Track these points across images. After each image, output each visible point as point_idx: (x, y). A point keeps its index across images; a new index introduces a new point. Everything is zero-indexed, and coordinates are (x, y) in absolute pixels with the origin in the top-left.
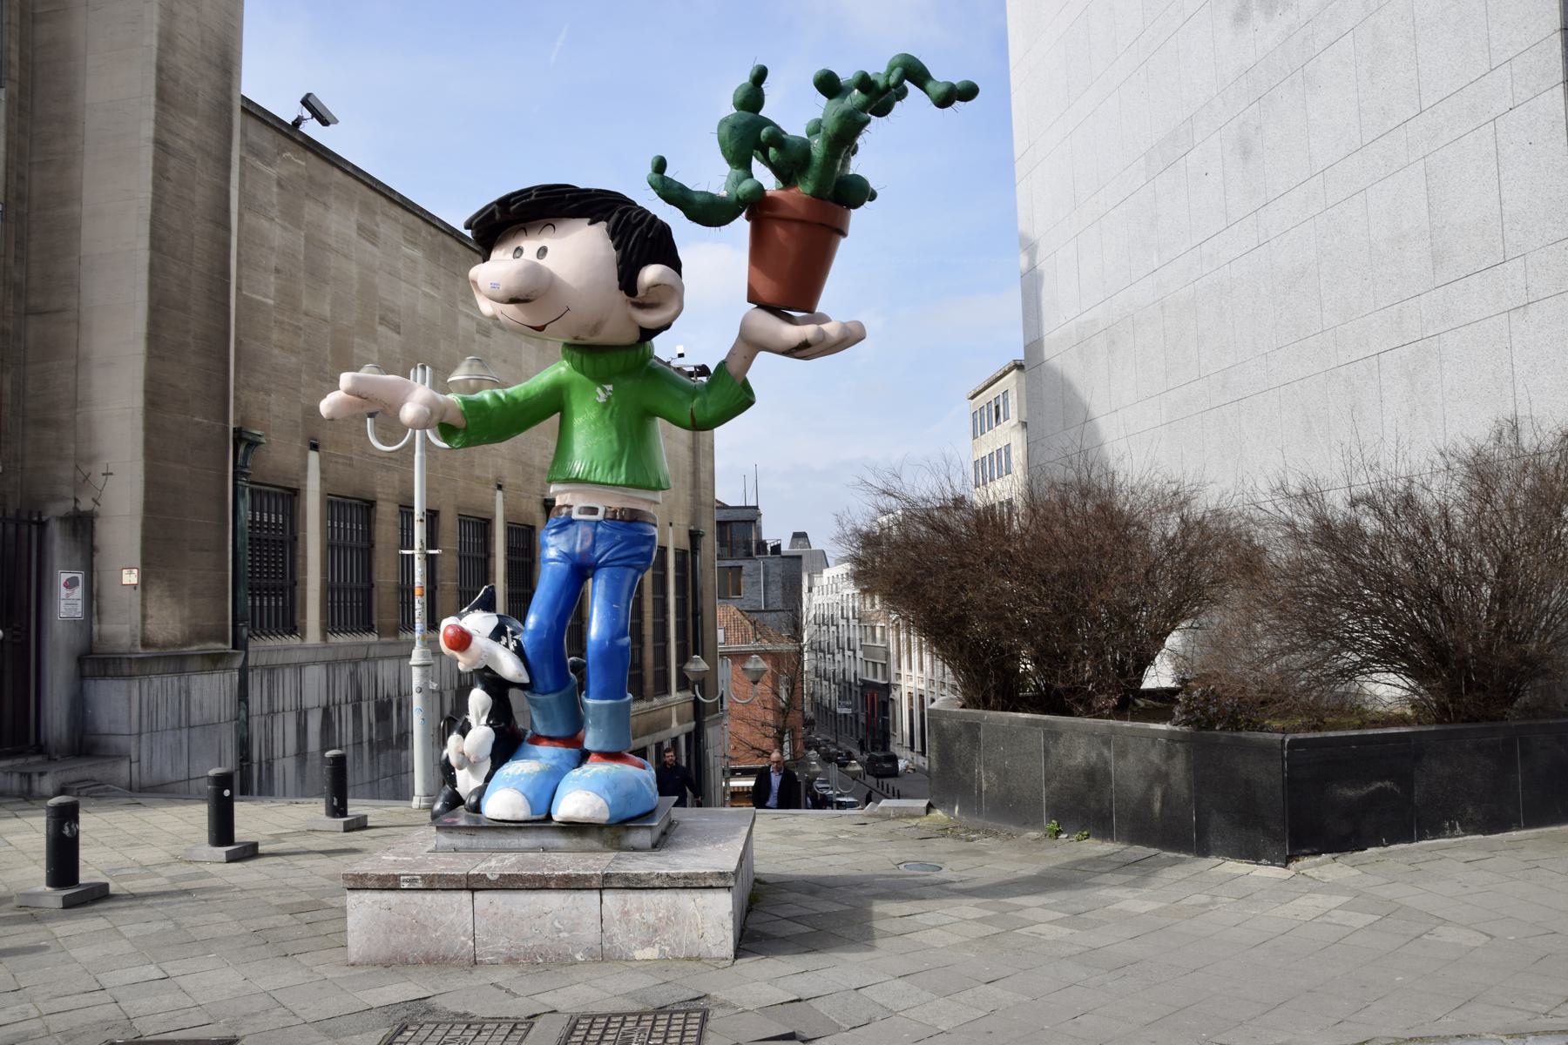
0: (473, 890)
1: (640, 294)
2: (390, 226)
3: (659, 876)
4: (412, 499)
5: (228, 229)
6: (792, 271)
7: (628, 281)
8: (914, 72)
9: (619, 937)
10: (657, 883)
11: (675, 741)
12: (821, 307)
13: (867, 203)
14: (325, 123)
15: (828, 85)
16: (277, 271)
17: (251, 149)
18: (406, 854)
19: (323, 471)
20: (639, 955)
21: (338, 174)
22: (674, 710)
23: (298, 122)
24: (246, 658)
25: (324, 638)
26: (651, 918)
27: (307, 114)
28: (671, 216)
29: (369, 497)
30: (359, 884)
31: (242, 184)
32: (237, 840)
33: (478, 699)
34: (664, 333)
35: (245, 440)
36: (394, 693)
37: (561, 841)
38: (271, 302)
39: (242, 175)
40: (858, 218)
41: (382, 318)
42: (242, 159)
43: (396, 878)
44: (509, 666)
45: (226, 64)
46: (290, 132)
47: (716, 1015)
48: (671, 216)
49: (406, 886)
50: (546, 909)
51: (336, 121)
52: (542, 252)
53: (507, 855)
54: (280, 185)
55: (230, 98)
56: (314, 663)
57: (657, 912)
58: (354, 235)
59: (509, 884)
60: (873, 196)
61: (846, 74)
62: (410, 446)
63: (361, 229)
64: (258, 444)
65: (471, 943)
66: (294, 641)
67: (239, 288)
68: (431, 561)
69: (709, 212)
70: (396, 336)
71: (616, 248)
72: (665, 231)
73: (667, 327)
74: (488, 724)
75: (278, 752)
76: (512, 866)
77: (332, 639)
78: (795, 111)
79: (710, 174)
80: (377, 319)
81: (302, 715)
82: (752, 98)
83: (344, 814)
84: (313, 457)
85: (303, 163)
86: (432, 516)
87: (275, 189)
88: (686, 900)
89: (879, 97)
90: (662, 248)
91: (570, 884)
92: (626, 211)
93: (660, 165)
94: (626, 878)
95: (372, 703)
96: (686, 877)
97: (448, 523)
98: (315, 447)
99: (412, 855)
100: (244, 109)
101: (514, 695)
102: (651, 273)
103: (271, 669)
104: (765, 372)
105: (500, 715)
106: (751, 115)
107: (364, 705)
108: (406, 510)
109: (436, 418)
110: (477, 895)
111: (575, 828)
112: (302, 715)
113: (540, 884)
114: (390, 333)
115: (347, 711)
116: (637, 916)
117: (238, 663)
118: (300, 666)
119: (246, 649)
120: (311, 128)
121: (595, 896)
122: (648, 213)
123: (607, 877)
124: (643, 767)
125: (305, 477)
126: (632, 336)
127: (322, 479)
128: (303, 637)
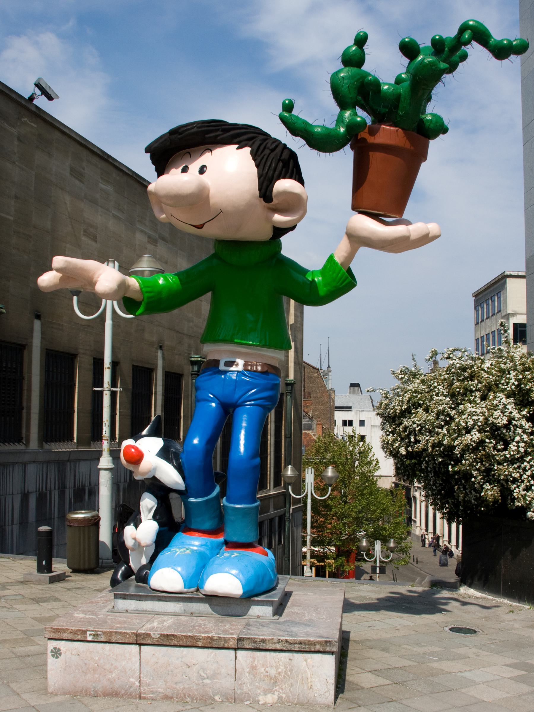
0: (140, 645)
1: (275, 201)
2: (91, 169)
3: (279, 641)
6: (385, 186)
7: (265, 191)
8: (481, 36)
10: (279, 647)
11: (271, 521)
13: (441, 136)
14: (50, 98)
15: (409, 50)
16: (16, 197)
18: (92, 613)
19: (43, 333)
20: (262, 699)
21: (58, 135)
23: (31, 99)
25: (41, 445)
27: (38, 92)
28: (296, 144)
33: (148, 503)
36: (87, 484)
37: (205, 607)
38: (11, 218)
43: (84, 632)
44: (170, 475)
48: (296, 144)
49: (90, 638)
50: (194, 661)
51: (58, 97)
52: (202, 170)
54: (19, 139)
56: (34, 462)
57: (277, 668)
59: (167, 641)
60: (445, 130)
61: (424, 42)
62: (102, 318)
63: (72, 170)
65: (137, 684)
66: (20, 447)
68: (113, 395)
69: (323, 143)
70: (93, 243)
71: (257, 166)
72: (293, 156)
73: (293, 228)
75: (7, 524)
76: (169, 627)
77: (46, 446)
78: (386, 66)
80: (82, 233)
81: (25, 496)
82: (354, 59)
83: (50, 570)
84: (37, 324)
85: (33, 126)
86: (115, 364)
87: (16, 143)
88: (300, 660)
89: (449, 54)
90: (291, 168)
91: (211, 645)
92: (265, 140)
93: (288, 107)
95: (72, 491)
97: (126, 368)
98: (38, 317)
99: (96, 614)
101: (173, 496)
102: (284, 185)
104: (365, 263)
105: (163, 515)
106: (355, 70)
107: (67, 491)
110: (142, 647)
111: (212, 599)
112: (25, 496)
114: (90, 242)
115: (56, 494)
116: (262, 670)
118: (24, 465)
120: (41, 102)
121: (232, 652)
122: (280, 142)
123: (240, 640)
125: (32, 337)
127: (42, 338)
128: (27, 444)
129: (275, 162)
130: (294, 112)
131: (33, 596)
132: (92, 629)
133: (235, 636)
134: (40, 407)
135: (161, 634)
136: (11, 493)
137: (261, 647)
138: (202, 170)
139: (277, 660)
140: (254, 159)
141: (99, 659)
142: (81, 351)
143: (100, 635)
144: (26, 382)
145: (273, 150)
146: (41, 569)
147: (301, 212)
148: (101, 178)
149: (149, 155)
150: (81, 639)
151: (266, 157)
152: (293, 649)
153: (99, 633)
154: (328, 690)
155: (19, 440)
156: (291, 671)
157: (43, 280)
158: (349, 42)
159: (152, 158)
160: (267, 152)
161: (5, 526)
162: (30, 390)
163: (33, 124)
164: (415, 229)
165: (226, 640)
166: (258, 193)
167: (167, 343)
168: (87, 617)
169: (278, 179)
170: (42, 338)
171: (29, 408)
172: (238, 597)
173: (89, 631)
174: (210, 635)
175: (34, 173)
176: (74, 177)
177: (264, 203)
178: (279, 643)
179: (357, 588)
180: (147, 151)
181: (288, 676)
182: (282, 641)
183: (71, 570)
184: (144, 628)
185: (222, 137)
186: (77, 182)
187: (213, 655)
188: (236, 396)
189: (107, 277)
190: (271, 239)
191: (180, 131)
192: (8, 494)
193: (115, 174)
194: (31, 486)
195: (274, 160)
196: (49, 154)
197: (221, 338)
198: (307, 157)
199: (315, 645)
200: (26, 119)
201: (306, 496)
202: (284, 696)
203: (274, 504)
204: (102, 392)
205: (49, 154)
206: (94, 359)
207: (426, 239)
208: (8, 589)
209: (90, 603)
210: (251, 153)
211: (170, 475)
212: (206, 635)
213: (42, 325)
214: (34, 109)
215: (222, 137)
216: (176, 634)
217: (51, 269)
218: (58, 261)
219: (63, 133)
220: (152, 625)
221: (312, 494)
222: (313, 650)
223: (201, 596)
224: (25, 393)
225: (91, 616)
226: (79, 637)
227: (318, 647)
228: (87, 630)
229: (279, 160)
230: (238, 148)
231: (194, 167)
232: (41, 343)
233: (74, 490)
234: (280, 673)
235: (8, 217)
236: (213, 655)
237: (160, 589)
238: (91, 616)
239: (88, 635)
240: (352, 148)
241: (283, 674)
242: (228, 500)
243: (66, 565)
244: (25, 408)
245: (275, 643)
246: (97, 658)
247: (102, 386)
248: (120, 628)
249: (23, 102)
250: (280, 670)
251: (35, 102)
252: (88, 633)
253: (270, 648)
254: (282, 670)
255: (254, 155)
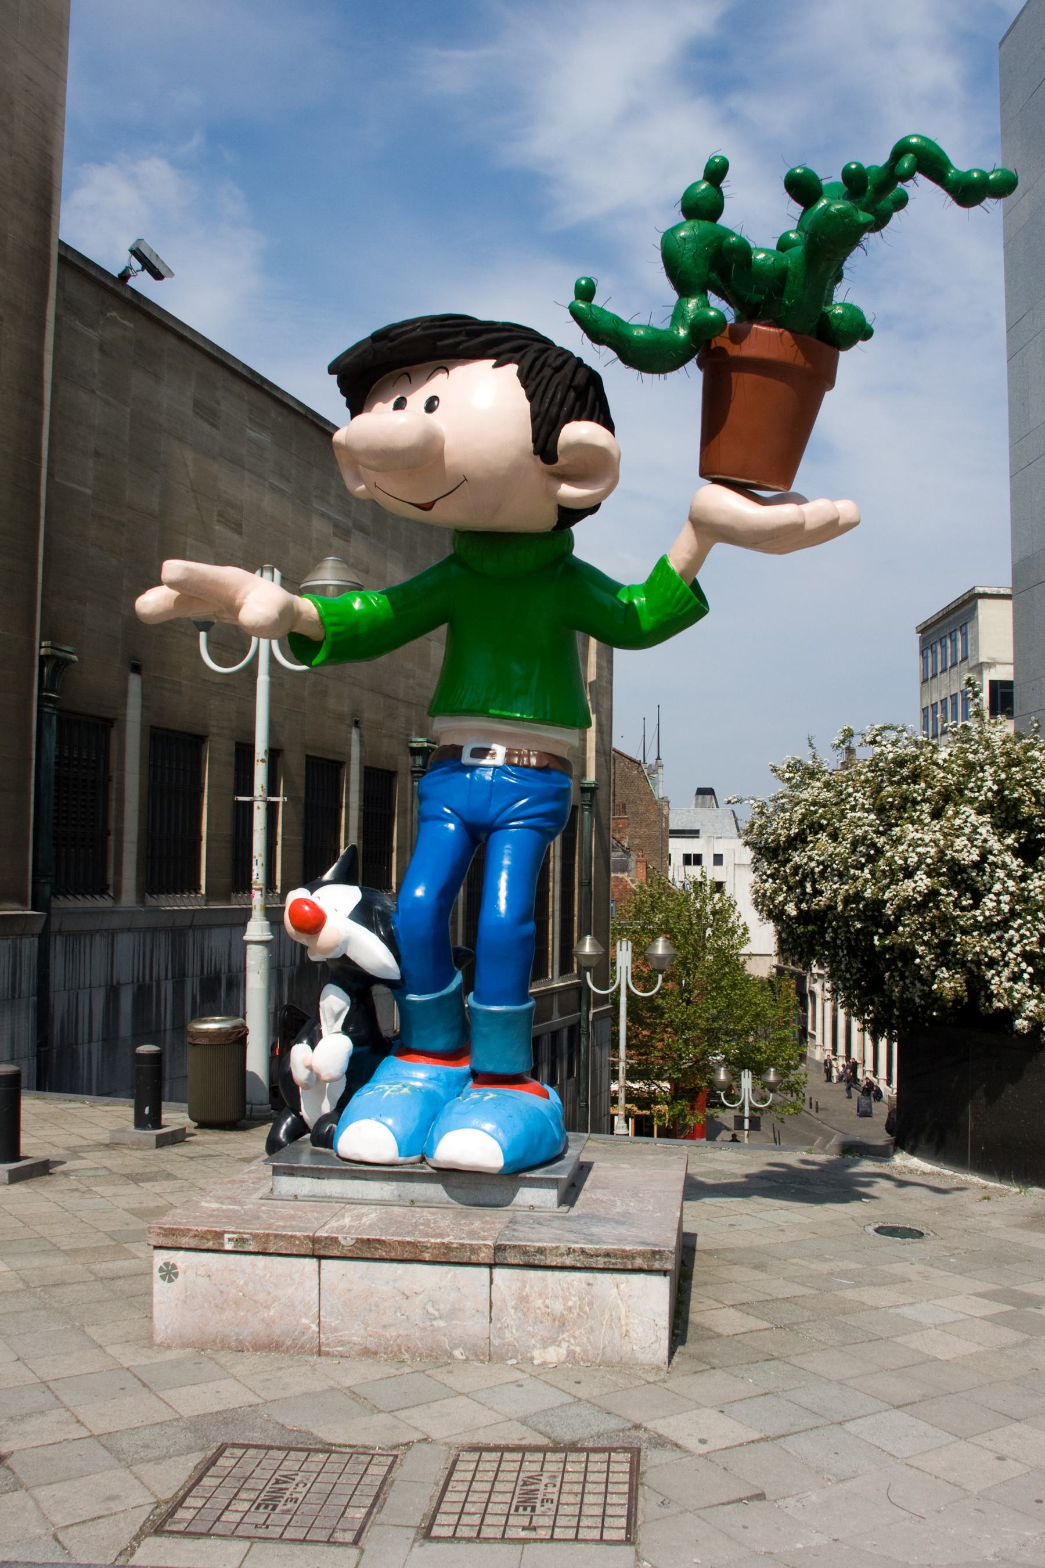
0: (320, 1258)
1: (562, 460)
3: (569, 1251)
4: (252, 734)
5: (41, 403)
7: (544, 444)
8: (931, 163)
9: (512, 1328)
10: (568, 1261)
12: (797, 486)
13: (860, 343)
14: (158, 276)
15: (802, 188)
16: (97, 454)
17: (64, 302)
18: (233, 1200)
19: (145, 697)
20: (538, 1356)
21: (172, 342)
22: (556, 999)
23: (124, 276)
24: (48, 922)
25: (141, 899)
26: (558, 1307)
27: (137, 265)
28: (599, 359)
29: (198, 730)
30: (172, 1240)
31: (56, 349)
32: (24, 1151)
33: (334, 1003)
34: (589, 518)
35: (56, 666)
36: (224, 968)
38: (88, 491)
39: (57, 336)
40: (850, 363)
41: (220, 515)
42: (58, 318)
43: (219, 1235)
44: (373, 953)
45: (43, 199)
46: (113, 290)
47: (652, 1458)
48: (599, 359)
49: (229, 1246)
51: (172, 274)
53: (365, 1209)
54: (102, 350)
55: (47, 244)
56: (129, 930)
57: (566, 1299)
58: (190, 413)
59: (368, 1251)
61: (830, 175)
62: (252, 670)
63: (198, 405)
64: (68, 662)
65: (314, 1327)
66: (103, 903)
67: (50, 474)
68: (271, 809)
69: (649, 356)
70: (236, 537)
71: (530, 397)
72: (594, 380)
73: (594, 509)
74: (345, 1029)
77: (151, 901)
78: (761, 219)
79: (647, 301)
80: (215, 517)
81: (113, 991)
82: (703, 207)
83: (157, 1124)
84: (135, 682)
86: (274, 754)
87: (97, 355)
89: (874, 195)
90: (591, 400)
93: (586, 292)
94: (523, 1250)
95: (197, 981)
96: (607, 1255)
97: (294, 761)
98: (136, 669)
100: (62, 259)
102: (578, 432)
103: (75, 936)
104: (723, 573)
106: (705, 225)
107: (189, 982)
108: (245, 752)
109: (285, 629)
110: (323, 1262)
112: (113, 991)
113: (410, 1255)
115: (168, 988)
117: (38, 928)
118: (112, 934)
119: (48, 909)
120: (141, 283)
121: (485, 1271)
124: (547, 1096)
125: (125, 705)
126: (547, 520)
128: (117, 897)
129: (562, 391)
130: (596, 301)
131: (128, 1171)
132: (233, 1229)
133: (490, 1243)
134: (140, 830)
135: (357, 1239)
136: (87, 985)
137: (536, 1262)
138: (431, 406)
139: (566, 1286)
140: (524, 385)
141: (246, 1284)
142: (214, 730)
143: (247, 1240)
144: (114, 786)
145: (558, 369)
146: (141, 1122)
147: (609, 481)
148: (250, 419)
149: (335, 377)
150: (214, 1248)
151: (545, 381)
152: (594, 1266)
153: (245, 1236)
154: (658, 1339)
155: (102, 891)
156: (591, 1304)
157: (146, 603)
158: (694, 175)
159: (341, 383)
160: (547, 372)
161: (76, 1044)
162: (121, 801)
163: (126, 323)
164: (814, 511)
165: (474, 1250)
166: (531, 446)
167: (367, 715)
168: (224, 1207)
169: (568, 421)
170: (144, 707)
171: (120, 833)
172: (496, 1172)
173: (229, 1232)
174: (446, 1240)
175: (129, 410)
176: (202, 417)
177: (541, 464)
178: (568, 1254)
179: (710, 1155)
180: (332, 370)
181: (585, 1313)
182: (574, 1251)
183: (196, 1124)
184: (327, 1227)
185: (465, 345)
186: (207, 427)
187: (449, 1276)
188: (493, 811)
189: (259, 597)
190: (554, 529)
191: (392, 334)
192: (81, 986)
193: (273, 412)
194: (124, 973)
195: (560, 387)
196: (156, 376)
197: (464, 706)
198: (619, 380)
199: (634, 1258)
200: (114, 314)
201: (618, 991)
202: (578, 1349)
203: (560, 1006)
204: (251, 804)
205: (156, 376)
206: (237, 744)
207: (833, 529)
208: (83, 1158)
209: (229, 1182)
210: (520, 374)
211: (373, 953)
212: (438, 1241)
213: (144, 684)
214: (128, 295)
215: (465, 345)
216: (383, 1238)
217: (159, 583)
218: (173, 568)
219: (182, 338)
220: (341, 1223)
221: (628, 987)
222: (630, 1267)
223: (429, 1170)
224: (113, 805)
225: (231, 1207)
226: (210, 1244)
227: (639, 1262)
228: (225, 1232)
229: (570, 387)
230: (495, 366)
231: (416, 400)
232: (142, 715)
233: (201, 980)
234: (570, 1309)
235: (82, 489)
236: (449, 1276)
237: (356, 1158)
238: (231, 1207)
239: (226, 1240)
240: (700, 365)
241: (576, 1311)
242: (477, 998)
243: (187, 1115)
244: (113, 833)
245: (562, 1255)
246: (242, 1282)
247: (251, 793)
248: (284, 1227)
249: (110, 284)
250: (570, 1303)
251: (131, 282)
252: (227, 1236)
253: (554, 1264)
254: (575, 1303)
255: (525, 377)
